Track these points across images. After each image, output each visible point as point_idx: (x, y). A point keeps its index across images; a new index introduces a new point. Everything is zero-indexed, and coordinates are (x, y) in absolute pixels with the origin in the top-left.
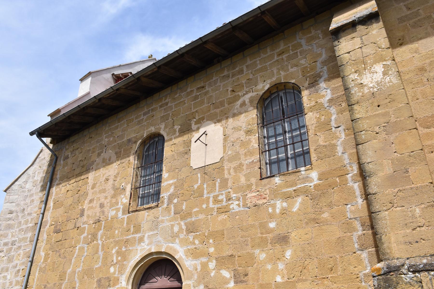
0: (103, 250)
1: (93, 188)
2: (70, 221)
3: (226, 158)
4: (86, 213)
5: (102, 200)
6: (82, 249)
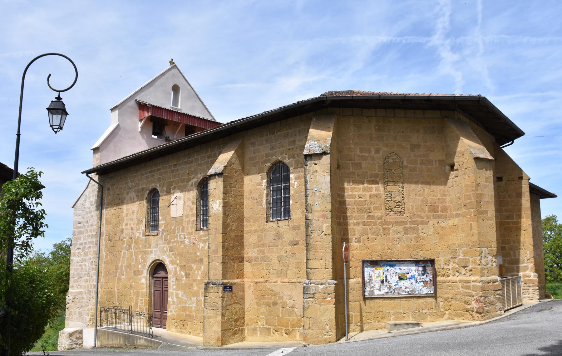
1: (127, 216)
4: (124, 231)
5: (132, 225)
6: (124, 253)
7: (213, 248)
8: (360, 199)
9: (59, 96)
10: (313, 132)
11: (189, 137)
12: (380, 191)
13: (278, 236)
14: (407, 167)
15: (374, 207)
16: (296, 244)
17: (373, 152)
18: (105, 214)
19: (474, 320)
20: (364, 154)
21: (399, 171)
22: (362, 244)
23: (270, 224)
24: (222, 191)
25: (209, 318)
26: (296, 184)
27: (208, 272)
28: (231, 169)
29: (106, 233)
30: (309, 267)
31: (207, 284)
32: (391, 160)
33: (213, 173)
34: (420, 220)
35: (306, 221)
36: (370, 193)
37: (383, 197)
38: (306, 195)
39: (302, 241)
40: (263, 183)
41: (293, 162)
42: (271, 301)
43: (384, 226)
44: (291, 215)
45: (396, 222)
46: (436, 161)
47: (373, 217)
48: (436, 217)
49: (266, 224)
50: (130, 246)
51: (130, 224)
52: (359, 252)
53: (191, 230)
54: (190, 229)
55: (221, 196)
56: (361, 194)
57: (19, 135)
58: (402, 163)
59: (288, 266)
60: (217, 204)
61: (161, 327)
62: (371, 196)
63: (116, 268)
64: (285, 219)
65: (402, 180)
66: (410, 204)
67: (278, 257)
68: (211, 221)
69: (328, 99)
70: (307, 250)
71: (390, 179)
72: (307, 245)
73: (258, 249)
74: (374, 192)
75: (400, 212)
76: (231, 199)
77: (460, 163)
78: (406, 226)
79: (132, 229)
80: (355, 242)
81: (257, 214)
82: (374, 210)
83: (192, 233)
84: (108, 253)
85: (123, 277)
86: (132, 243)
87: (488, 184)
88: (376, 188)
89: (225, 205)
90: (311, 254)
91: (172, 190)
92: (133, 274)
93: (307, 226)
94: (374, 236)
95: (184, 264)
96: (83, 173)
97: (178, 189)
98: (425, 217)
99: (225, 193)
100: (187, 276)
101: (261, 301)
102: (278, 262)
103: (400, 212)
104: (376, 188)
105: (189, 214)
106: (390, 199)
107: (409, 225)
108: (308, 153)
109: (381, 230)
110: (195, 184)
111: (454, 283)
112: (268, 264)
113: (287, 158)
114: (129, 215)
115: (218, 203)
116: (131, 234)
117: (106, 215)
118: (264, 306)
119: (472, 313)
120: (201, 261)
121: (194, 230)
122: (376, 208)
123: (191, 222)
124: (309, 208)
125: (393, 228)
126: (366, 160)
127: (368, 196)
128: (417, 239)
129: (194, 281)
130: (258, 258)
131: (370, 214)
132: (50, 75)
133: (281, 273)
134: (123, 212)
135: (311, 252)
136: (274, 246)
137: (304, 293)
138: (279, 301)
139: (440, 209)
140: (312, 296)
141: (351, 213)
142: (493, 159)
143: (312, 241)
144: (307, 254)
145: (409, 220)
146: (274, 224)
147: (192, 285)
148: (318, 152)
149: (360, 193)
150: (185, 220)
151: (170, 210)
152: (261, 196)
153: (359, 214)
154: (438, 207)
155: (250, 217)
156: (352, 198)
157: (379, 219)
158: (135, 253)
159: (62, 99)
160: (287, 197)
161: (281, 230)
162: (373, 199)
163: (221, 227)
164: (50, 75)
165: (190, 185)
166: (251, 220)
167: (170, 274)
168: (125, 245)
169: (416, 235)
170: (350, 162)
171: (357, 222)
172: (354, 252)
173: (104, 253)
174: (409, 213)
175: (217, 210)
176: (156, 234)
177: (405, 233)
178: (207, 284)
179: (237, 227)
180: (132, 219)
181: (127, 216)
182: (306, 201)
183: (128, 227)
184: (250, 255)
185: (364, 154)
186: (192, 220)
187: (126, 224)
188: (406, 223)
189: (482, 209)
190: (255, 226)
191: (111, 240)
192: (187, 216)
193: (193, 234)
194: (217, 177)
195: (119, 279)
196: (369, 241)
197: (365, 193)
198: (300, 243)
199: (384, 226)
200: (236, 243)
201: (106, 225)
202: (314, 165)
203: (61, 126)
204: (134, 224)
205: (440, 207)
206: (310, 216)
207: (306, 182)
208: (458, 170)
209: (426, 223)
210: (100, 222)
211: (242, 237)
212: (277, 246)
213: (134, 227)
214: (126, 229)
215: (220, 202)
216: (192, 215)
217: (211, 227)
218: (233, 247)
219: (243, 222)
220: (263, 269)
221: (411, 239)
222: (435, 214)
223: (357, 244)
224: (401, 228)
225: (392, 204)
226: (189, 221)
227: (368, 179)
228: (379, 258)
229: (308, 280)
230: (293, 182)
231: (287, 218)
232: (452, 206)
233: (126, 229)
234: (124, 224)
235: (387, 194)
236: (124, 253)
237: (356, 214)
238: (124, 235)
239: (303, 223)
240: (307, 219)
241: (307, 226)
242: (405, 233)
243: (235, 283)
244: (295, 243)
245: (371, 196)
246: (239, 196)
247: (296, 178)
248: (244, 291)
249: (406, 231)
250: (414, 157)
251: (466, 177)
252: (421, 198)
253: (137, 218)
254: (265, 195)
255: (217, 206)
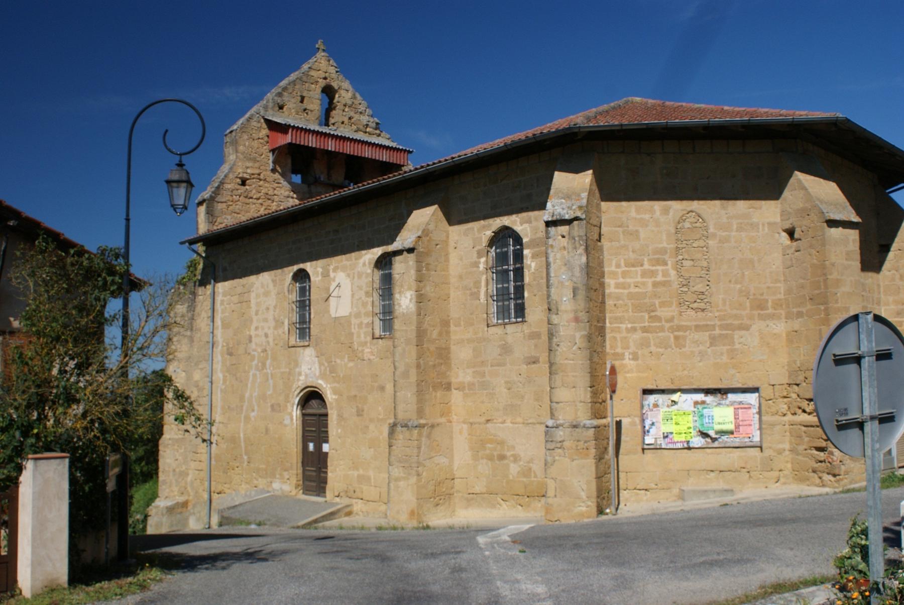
0: (272, 378)
1: (257, 314)
2: (105, 385)
3: (353, 314)
4: (254, 339)
5: (266, 330)
6: (254, 375)
7: (401, 368)
8: (637, 290)
9: (180, 161)
10: (561, 180)
11: (359, 187)
12: (669, 276)
13: (506, 349)
14: (714, 235)
15: (659, 303)
16: (534, 363)
17: (658, 213)
18: (220, 311)
19: (823, 486)
20: (643, 216)
21: (702, 243)
22: (640, 362)
23: (492, 330)
24: (414, 277)
25: (397, 479)
26: (533, 265)
27: (395, 407)
28: (428, 241)
29: (223, 342)
30: (555, 399)
31: (393, 426)
32: (687, 225)
33: (400, 248)
34: (736, 322)
35: (549, 328)
36: (653, 279)
37: (675, 285)
38: (548, 287)
39: (544, 357)
40: (479, 263)
41: (528, 229)
42: (495, 453)
43: (676, 333)
44: (526, 315)
45: (697, 327)
46: (763, 225)
47: (658, 319)
48: (762, 318)
49: (486, 328)
50: (264, 365)
51: (263, 328)
52: (635, 375)
53: (365, 338)
54: (362, 336)
55: (414, 285)
56: (638, 282)
57: (128, 220)
58: (706, 229)
59: (523, 397)
60: (406, 297)
61: (318, 495)
62: (655, 284)
63: (242, 399)
64: (517, 322)
65: (706, 257)
66: (721, 296)
67: (506, 382)
68: (397, 325)
69: (581, 130)
70: (550, 373)
71: (686, 257)
72: (551, 365)
73: (473, 370)
74: (660, 278)
75: (703, 310)
76: (429, 289)
77: (804, 228)
78: (713, 332)
79: (266, 336)
80: (629, 359)
81: (472, 314)
82: (660, 307)
83: (366, 343)
84: (227, 374)
85: (252, 414)
86: (267, 358)
87: (850, 263)
88: (663, 271)
89: (420, 299)
90: (558, 378)
91: (331, 271)
92: (269, 410)
93: (551, 335)
94: (660, 350)
95: (353, 393)
96: (182, 243)
97: (341, 271)
98: (745, 318)
99: (420, 279)
100: (360, 413)
101: (480, 454)
102: (505, 390)
103: (703, 310)
104: (663, 271)
105: (360, 313)
106: (687, 289)
107: (717, 332)
108: (550, 219)
109: (672, 339)
110: (370, 263)
111: (795, 426)
112: (490, 394)
113: (518, 223)
114: (260, 312)
115: (409, 297)
116: (264, 344)
117: (223, 312)
118: (485, 461)
119: (820, 475)
120: (382, 388)
121: (369, 338)
122: (663, 304)
123: (364, 326)
124: (553, 307)
125: (691, 337)
126: (647, 226)
127: (650, 285)
128: (732, 353)
129: (371, 420)
130: (473, 384)
131: (653, 314)
132: (167, 131)
133: (511, 409)
134: (251, 308)
135: (557, 376)
136: (499, 365)
137: (547, 441)
138: (509, 454)
139: (770, 304)
140: (559, 445)
141: (623, 312)
142: (860, 220)
143: (559, 359)
144: (550, 379)
145: (718, 323)
146: (499, 330)
147: (367, 427)
148: (567, 217)
149: (637, 280)
150: (354, 321)
151: (329, 306)
152: (477, 284)
153: (636, 314)
154: (767, 301)
155: (459, 318)
156: (624, 288)
157: (667, 321)
158: (272, 375)
159: (184, 165)
160: (519, 286)
161: (510, 339)
162: (659, 290)
163: (415, 335)
164: (167, 131)
165: (361, 265)
166: (462, 323)
167: (332, 409)
168: (255, 362)
169: (729, 347)
170: (620, 230)
171: (632, 327)
172: (628, 375)
173: (221, 375)
174: (718, 311)
175: (407, 307)
176: (307, 344)
177: (711, 345)
178: (393, 427)
179: (440, 334)
180: (266, 320)
181: (257, 314)
182: (549, 296)
183: (260, 332)
184: (461, 379)
185: (643, 216)
186: (365, 321)
187: (257, 328)
188: (713, 327)
189: (839, 305)
190: (469, 332)
191: (231, 354)
192: (358, 315)
193: (369, 344)
194: (405, 253)
195: (247, 418)
196: (653, 358)
197: (645, 280)
198: (541, 360)
199: (676, 333)
200: (437, 361)
201: (222, 328)
202: (560, 237)
203: (186, 204)
204: (269, 328)
205: (770, 301)
206: (555, 319)
207: (548, 265)
208: (800, 239)
209: (747, 328)
210: (212, 324)
211: (447, 349)
212: (504, 365)
213: (270, 332)
214: (257, 336)
215: (411, 295)
216: (366, 314)
217: (397, 334)
218: (434, 366)
219: (450, 326)
220: (483, 402)
221: (722, 354)
222: (762, 312)
223: (632, 362)
224: (704, 336)
225: (690, 297)
226: (361, 323)
227: (651, 257)
228: (654, 387)
229: (553, 421)
230: (529, 263)
231: (519, 320)
232: (790, 299)
233: (257, 336)
234: (253, 328)
235: (681, 280)
236: (254, 375)
237: (631, 314)
238: (253, 346)
239: (544, 330)
240: (549, 323)
241: (551, 335)
242: (711, 345)
243: (438, 425)
244: (533, 360)
245: (655, 284)
246: (443, 283)
247: (534, 256)
248: (451, 438)
249: (713, 341)
250: (728, 218)
251: (814, 252)
252: (739, 286)
253: (274, 319)
254: (483, 283)
255: (408, 301)
